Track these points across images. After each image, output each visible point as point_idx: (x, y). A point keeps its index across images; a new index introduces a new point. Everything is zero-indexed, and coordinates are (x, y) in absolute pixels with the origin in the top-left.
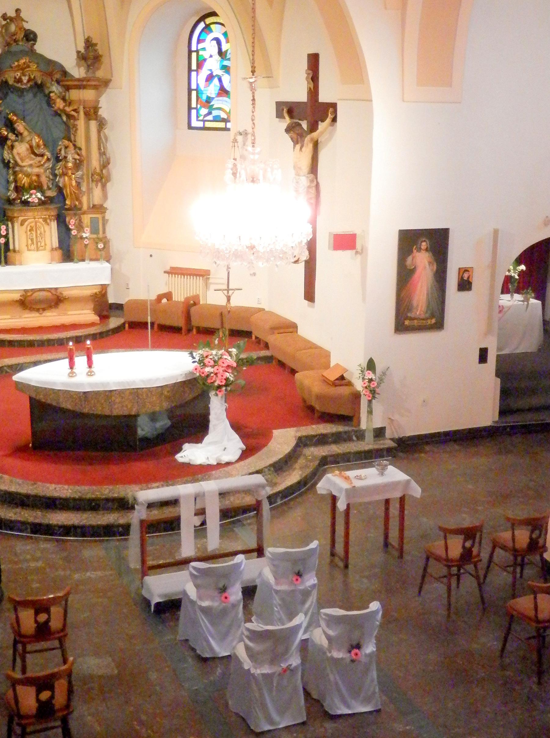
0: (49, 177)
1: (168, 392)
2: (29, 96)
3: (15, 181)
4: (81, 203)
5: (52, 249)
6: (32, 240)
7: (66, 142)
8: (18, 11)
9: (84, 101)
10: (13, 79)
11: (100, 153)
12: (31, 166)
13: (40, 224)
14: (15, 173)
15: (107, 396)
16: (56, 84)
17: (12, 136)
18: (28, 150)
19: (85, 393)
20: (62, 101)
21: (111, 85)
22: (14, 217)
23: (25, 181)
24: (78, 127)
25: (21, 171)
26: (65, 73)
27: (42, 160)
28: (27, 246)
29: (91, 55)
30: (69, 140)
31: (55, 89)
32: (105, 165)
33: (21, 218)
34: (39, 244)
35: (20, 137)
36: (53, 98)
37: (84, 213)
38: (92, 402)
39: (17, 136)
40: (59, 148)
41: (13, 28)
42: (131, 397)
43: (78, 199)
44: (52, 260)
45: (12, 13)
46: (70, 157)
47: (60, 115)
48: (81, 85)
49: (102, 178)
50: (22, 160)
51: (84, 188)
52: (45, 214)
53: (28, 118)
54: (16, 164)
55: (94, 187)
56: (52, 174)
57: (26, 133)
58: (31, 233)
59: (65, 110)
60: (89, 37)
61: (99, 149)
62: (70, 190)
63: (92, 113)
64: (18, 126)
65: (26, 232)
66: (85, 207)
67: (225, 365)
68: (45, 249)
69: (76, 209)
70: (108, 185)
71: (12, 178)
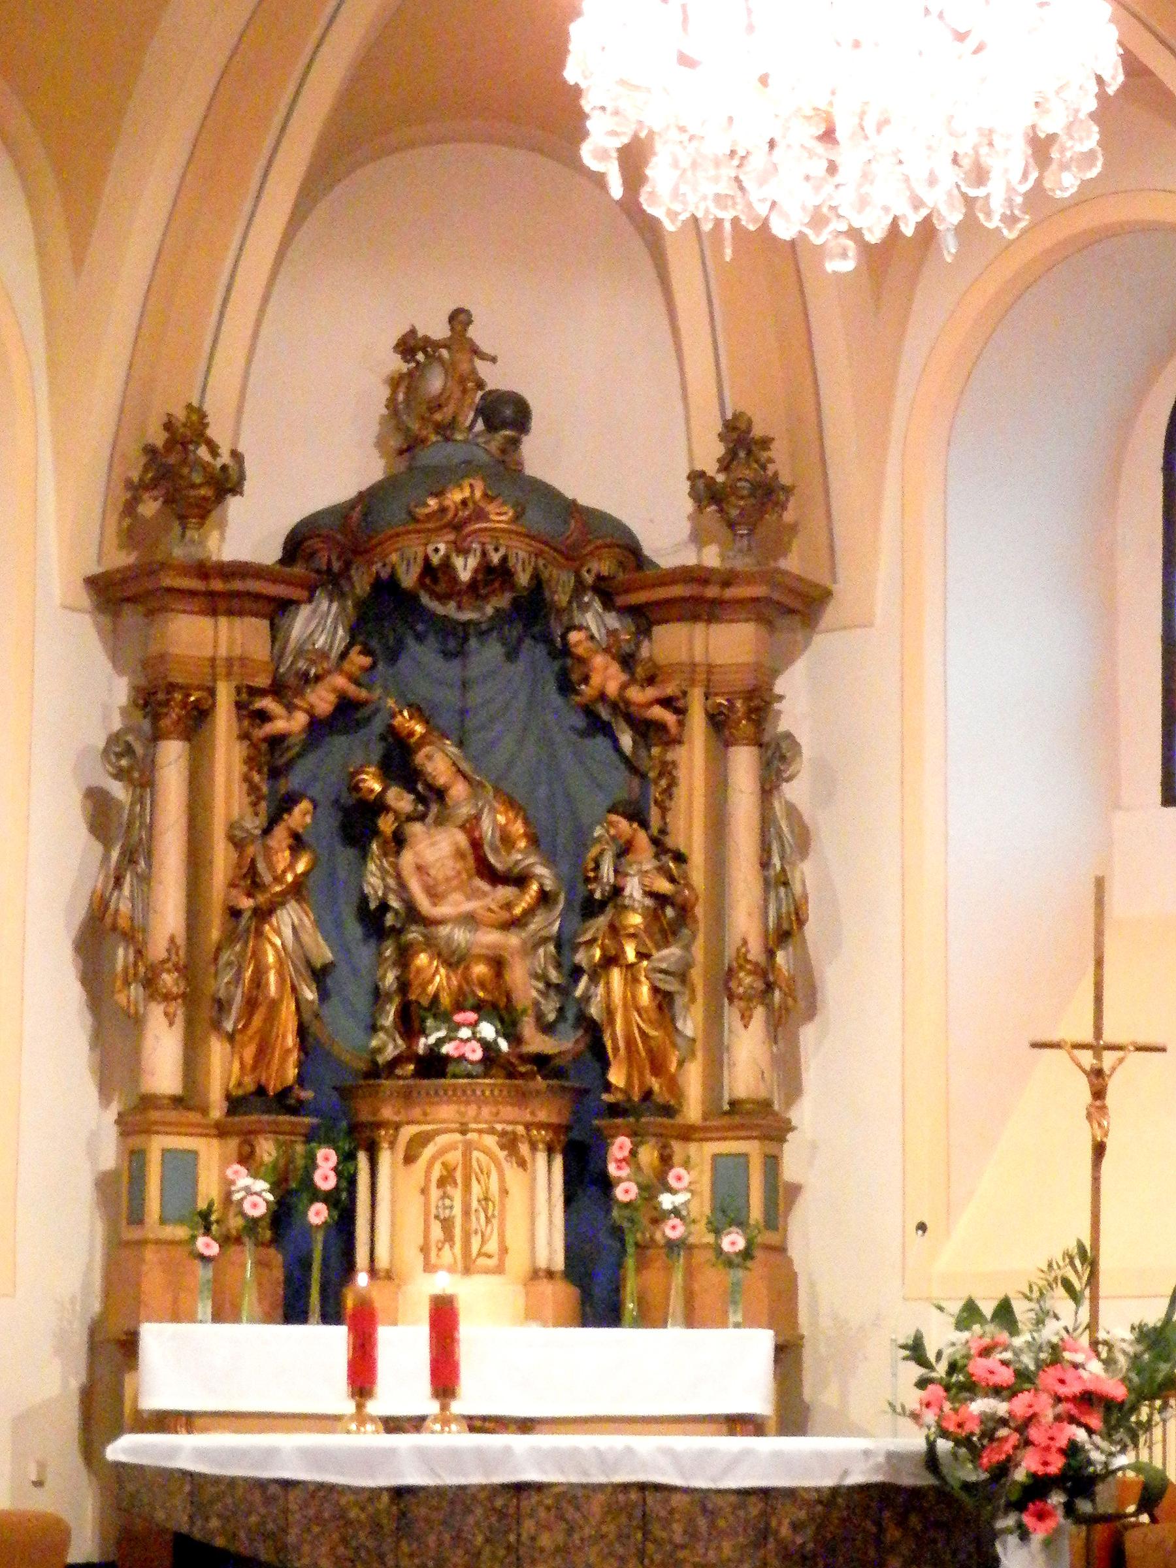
0: (543, 977)
1: (796, 1527)
2: (487, 654)
3: (404, 986)
4: (674, 1085)
5: (535, 1274)
6: (447, 1224)
7: (623, 824)
8: (459, 318)
9: (710, 668)
10: (416, 570)
11: (766, 883)
12: (470, 920)
13: (482, 1157)
14: (404, 956)
15: (502, 1515)
16: (597, 605)
17: (401, 800)
18: (460, 854)
19: (399, 1493)
20: (615, 668)
21: (830, 614)
22: (379, 1125)
23: (438, 980)
24: (681, 774)
25: (430, 943)
26: (631, 552)
27: (519, 898)
28: (425, 1250)
29: (746, 485)
30: (638, 816)
31: (594, 623)
32: (786, 931)
33: (408, 1132)
34: (475, 1243)
35: (435, 808)
36: (580, 651)
37: (687, 1134)
38: (432, 1540)
39: (420, 799)
40: (594, 852)
41: (435, 382)
42: (610, 1529)
43: (657, 1066)
44: (532, 1314)
45: (438, 330)
46: (633, 888)
47: (606, 730)
48: (699, 596)
49: (777, 985)
50: (435, 896)
51: (690, 1024)
52: (513, 1116)
53: (477, 741)
54: (413, 914)
55: (738, 1024)
56: (559, 966)
57: (459, 790)
58: (445, 1196)
59: (628, 703)
60: (737, 416)
61: (765, 864)
62: (627, 1022)
63: (746, 714)
64: (429, 757)
65: (424, 1191)
66: (693, 1111)
67: (1073, 1388)
68: (499, 1270)
69: (652, 1112)
70: (808, 1034)
71: (390, 979)
